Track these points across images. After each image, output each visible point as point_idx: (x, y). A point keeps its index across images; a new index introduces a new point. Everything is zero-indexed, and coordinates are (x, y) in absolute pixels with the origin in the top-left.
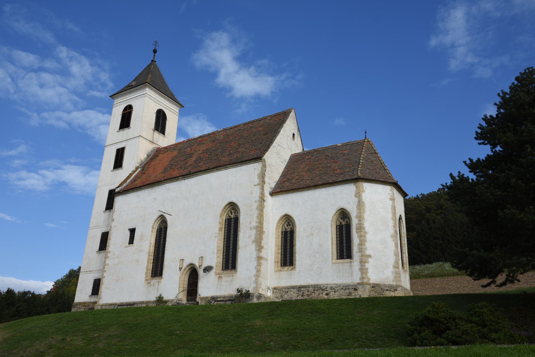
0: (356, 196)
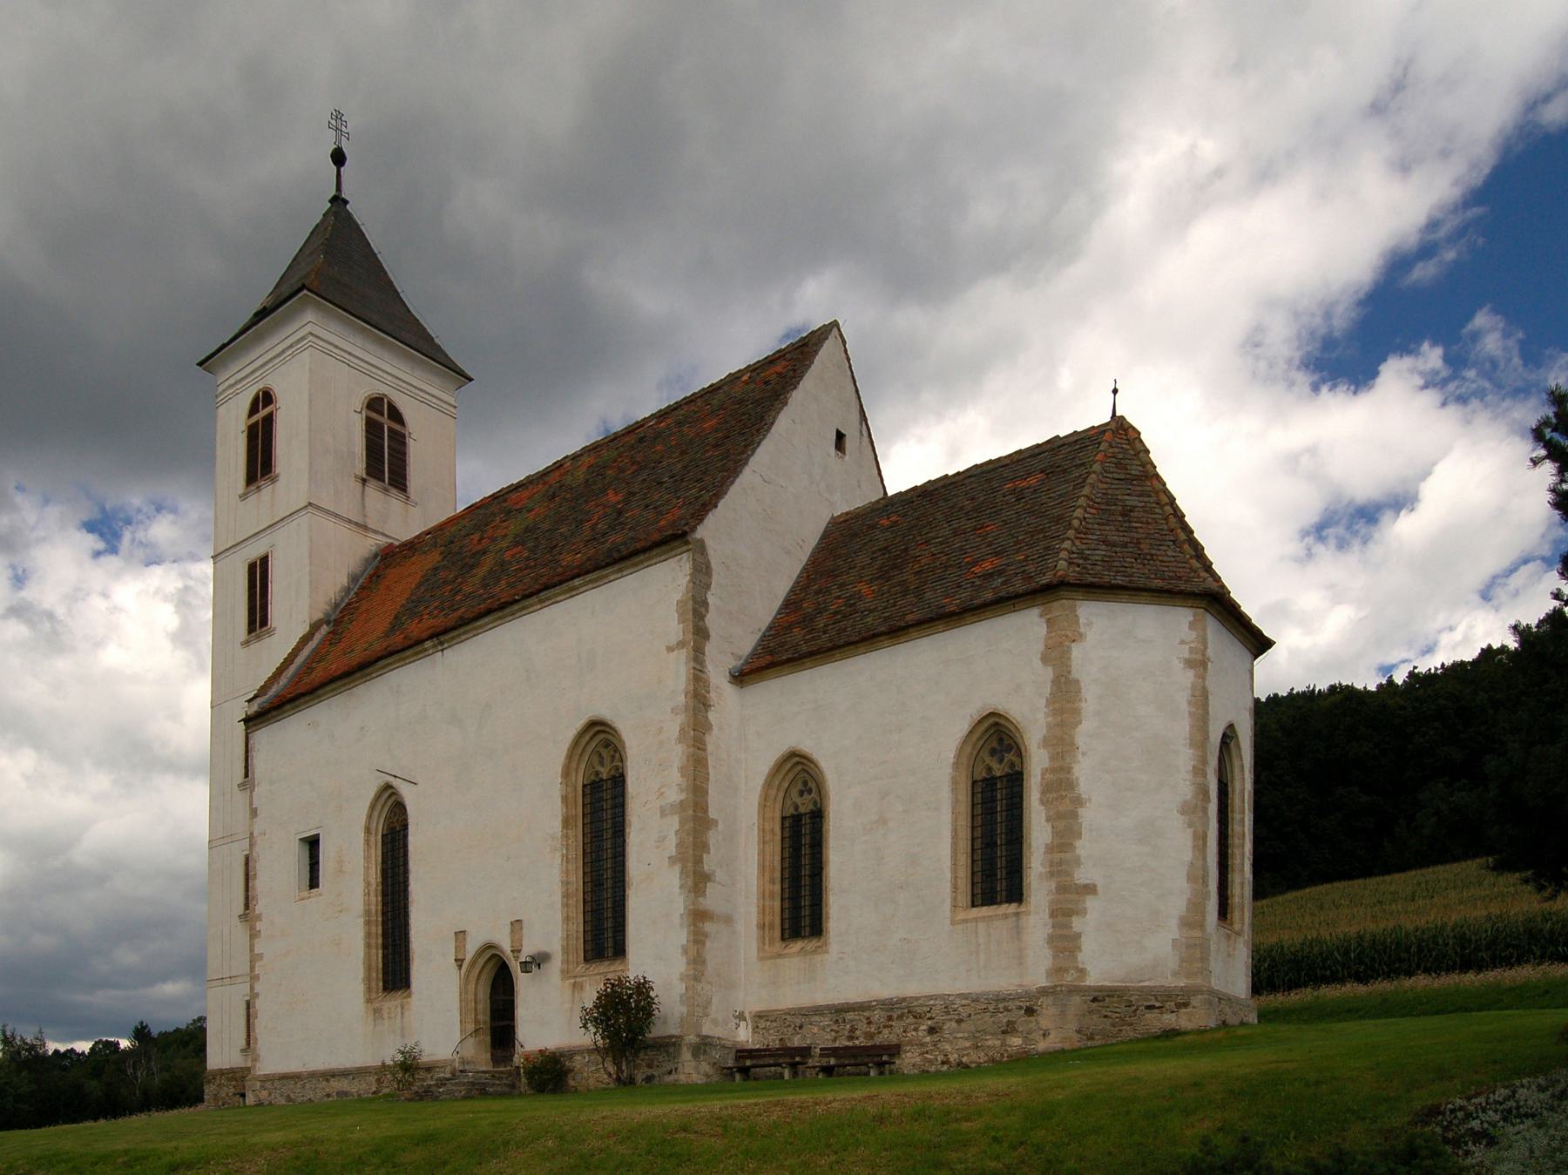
0: (1045, 659)
